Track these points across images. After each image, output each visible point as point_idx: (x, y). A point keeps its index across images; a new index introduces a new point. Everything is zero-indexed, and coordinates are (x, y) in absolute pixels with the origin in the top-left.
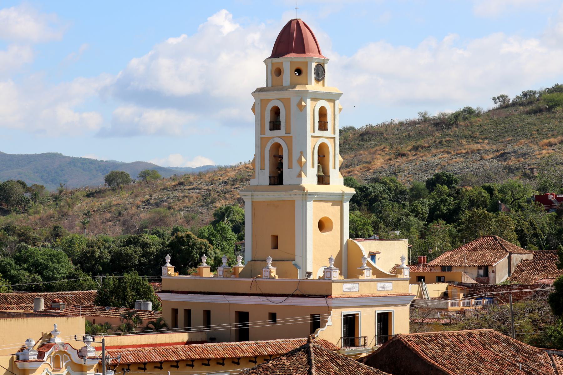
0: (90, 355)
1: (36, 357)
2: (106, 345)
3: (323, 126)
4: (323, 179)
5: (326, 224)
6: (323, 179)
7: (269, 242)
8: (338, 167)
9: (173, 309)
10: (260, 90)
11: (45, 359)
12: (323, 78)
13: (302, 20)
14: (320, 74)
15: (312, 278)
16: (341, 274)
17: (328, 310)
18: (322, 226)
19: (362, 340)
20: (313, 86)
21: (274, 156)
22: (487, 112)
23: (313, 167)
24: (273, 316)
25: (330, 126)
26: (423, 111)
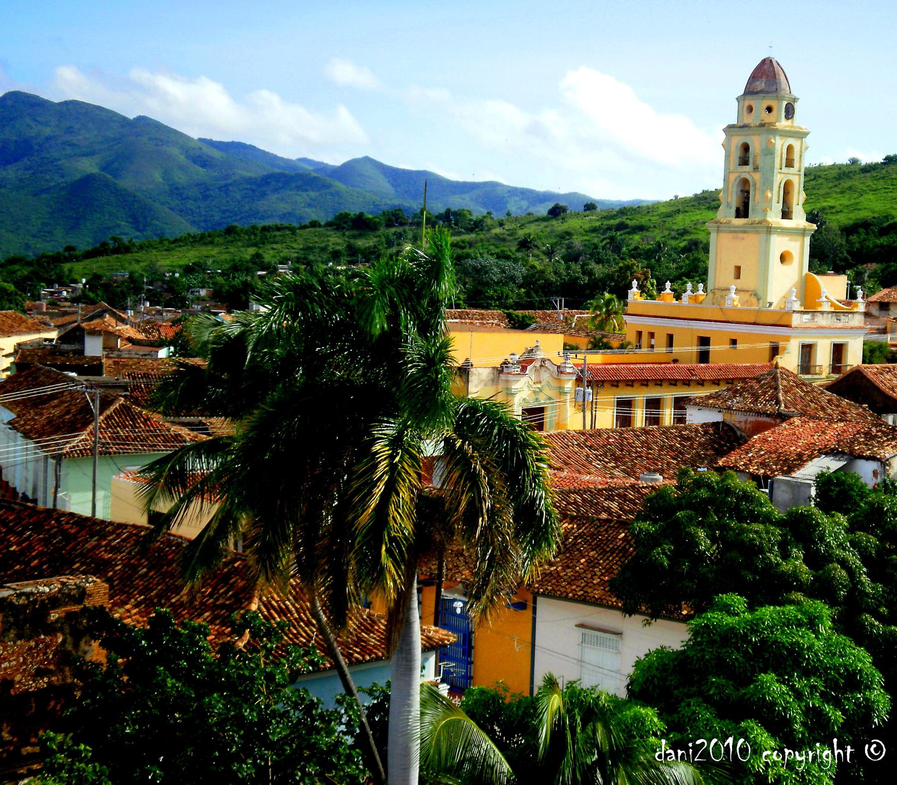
0: (568, 370)
1: (519, 370)
2: (587, 362)
3: (789, 163)
4: (786, 214)
5: (787, 258)
6: (786, 214)
7: (732, 272)
8: (801, 203)
9: (668, 334)
10: (730, 127)
11: (527, 372)
12: (793, 117)
13: (776, 59)
14: (790, 112)
15: (772, 308)
16: (801, 305)
17: (787, 339)
18: (783, 258)
19: (817, 368)
20: (783, 124)
21: (742, 191)
22: (12, 332)
23: (778, 203)
24: (734, 342)
25: (796, 164)
26: (676, 194)
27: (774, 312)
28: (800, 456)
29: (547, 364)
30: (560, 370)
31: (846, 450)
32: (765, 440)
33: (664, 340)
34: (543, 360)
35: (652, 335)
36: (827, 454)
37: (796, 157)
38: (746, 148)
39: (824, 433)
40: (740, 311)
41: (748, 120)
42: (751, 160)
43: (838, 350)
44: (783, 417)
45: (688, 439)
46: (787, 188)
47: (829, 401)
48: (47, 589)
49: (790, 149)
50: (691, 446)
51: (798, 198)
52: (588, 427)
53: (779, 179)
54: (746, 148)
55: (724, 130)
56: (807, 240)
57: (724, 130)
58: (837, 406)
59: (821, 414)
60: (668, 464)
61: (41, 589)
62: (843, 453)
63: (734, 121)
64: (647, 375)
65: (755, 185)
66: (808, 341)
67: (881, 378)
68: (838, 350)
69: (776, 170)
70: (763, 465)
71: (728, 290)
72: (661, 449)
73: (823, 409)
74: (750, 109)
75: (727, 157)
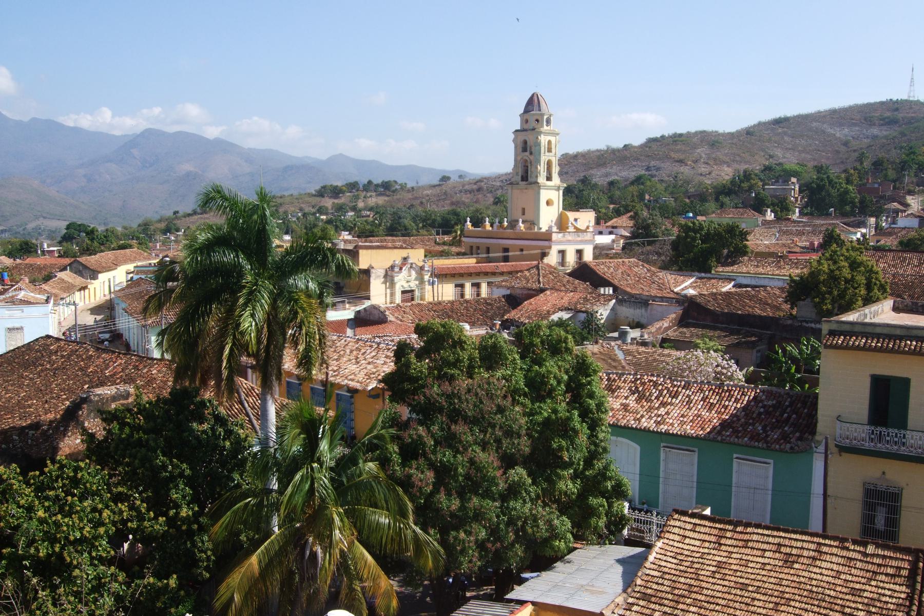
3: (550, 150)
4: (549, 178)
6: (549, 178)
10: (517, 131)
14: (548, 122)
27: (543, 233)
28: (548, 312)
29: (414, 266)
30: (422, 268)
31: (573, 307)
32: (531, 304)
33: (485, 251)
34: (412, 264)
35: (478, 248)
36: (562, 310)
37: (553, 146)
38: (525, 142)
39: (562, 298)
40: (524, 233)
41: (526, 127)
42: (528, 149)
43: (580, 253)
44: (542, 291)
45: (490, 304)
46: (549, 164)
47: (568, 281)
48: (109, 392)
49: (549, 142)
50: (492, 309)
51: (555, 170)
52: (436, 299)
53: (544, 158)
54: (525, 142)
55: (513, 133)
56: (561, 192)
57: (513, 133)
58: (573, 284)
59: (563, 288)
60: (478, 318)
61: (106, 392)
62: (571, 309)
63: (519, 128)
64: (472, 271)
65: (531, 163)
66: (579, 247)
67: (598, 267)
68: (580, 253)
69: (542, 155)
70: (529, 318)
71: (518, 221)
72: (475, 310)
73: (564, 286)
74: (527, 121)
75: (516, 147)
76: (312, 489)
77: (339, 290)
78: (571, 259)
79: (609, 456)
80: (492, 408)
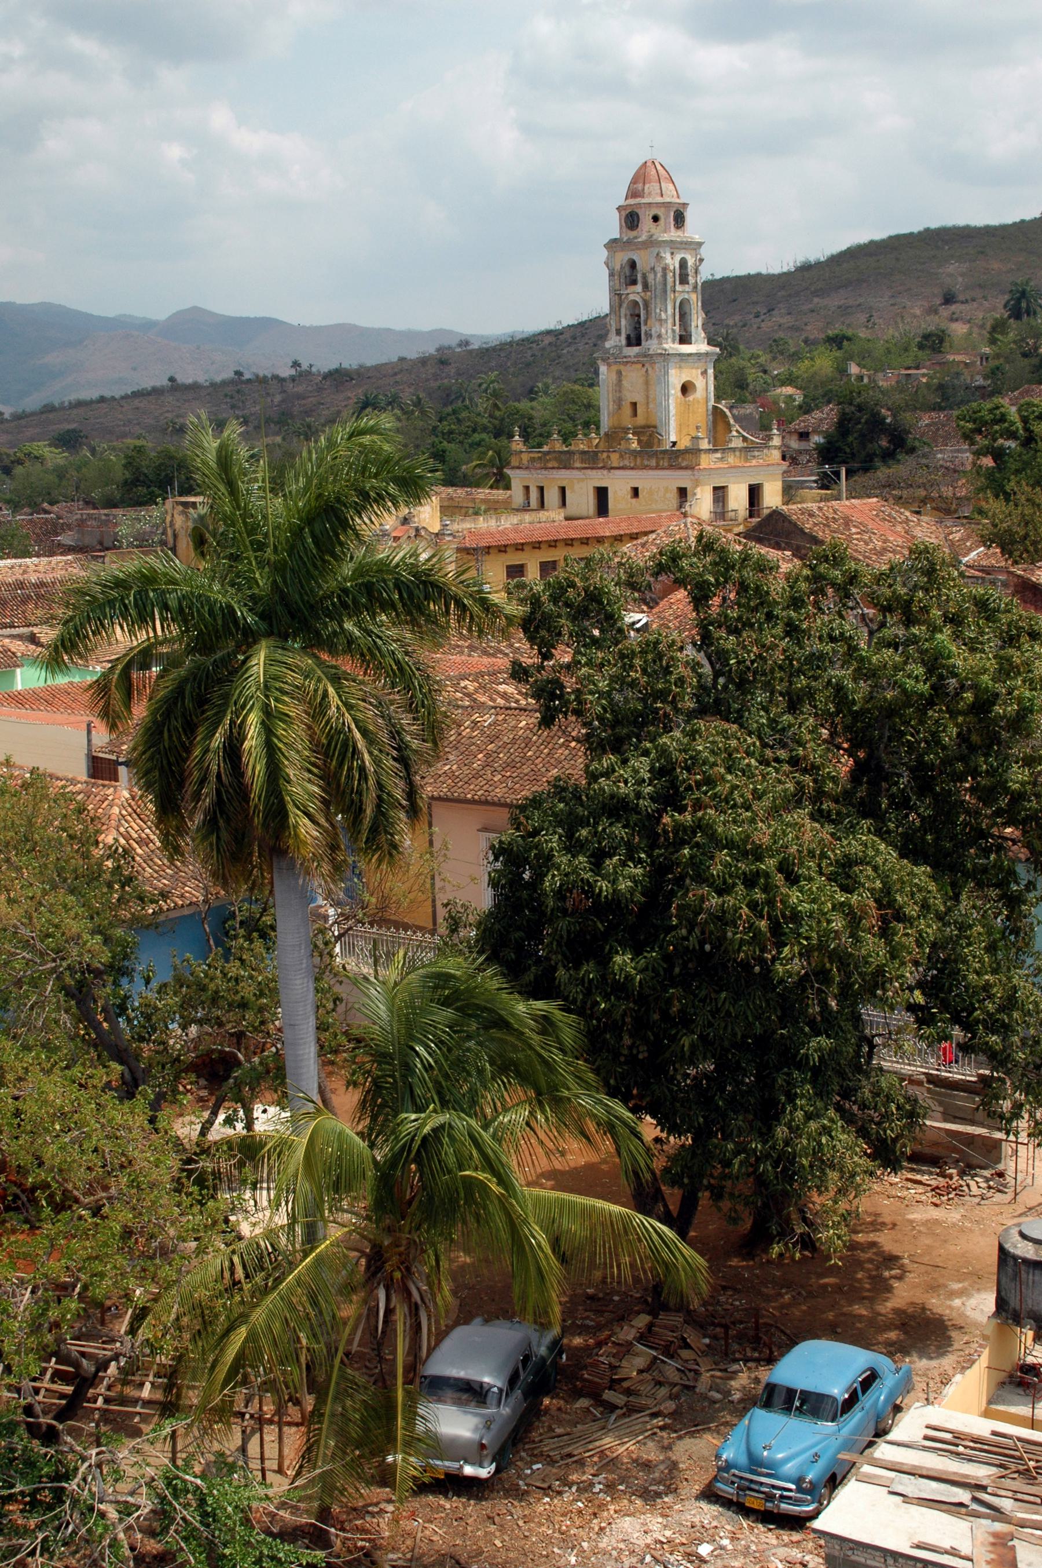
3: (684, 280)
10: (614, 241)
43: (755, 493)
49: (683, 263)
51: (697, 320)
54: (633, 265)
76: (431, 1198)
77: (761, 1134)
78: (738, 499)
79: (622, 202)
80: (504, 696)
